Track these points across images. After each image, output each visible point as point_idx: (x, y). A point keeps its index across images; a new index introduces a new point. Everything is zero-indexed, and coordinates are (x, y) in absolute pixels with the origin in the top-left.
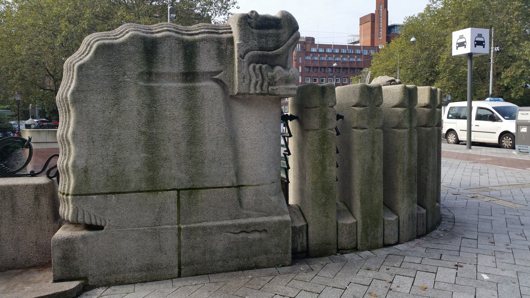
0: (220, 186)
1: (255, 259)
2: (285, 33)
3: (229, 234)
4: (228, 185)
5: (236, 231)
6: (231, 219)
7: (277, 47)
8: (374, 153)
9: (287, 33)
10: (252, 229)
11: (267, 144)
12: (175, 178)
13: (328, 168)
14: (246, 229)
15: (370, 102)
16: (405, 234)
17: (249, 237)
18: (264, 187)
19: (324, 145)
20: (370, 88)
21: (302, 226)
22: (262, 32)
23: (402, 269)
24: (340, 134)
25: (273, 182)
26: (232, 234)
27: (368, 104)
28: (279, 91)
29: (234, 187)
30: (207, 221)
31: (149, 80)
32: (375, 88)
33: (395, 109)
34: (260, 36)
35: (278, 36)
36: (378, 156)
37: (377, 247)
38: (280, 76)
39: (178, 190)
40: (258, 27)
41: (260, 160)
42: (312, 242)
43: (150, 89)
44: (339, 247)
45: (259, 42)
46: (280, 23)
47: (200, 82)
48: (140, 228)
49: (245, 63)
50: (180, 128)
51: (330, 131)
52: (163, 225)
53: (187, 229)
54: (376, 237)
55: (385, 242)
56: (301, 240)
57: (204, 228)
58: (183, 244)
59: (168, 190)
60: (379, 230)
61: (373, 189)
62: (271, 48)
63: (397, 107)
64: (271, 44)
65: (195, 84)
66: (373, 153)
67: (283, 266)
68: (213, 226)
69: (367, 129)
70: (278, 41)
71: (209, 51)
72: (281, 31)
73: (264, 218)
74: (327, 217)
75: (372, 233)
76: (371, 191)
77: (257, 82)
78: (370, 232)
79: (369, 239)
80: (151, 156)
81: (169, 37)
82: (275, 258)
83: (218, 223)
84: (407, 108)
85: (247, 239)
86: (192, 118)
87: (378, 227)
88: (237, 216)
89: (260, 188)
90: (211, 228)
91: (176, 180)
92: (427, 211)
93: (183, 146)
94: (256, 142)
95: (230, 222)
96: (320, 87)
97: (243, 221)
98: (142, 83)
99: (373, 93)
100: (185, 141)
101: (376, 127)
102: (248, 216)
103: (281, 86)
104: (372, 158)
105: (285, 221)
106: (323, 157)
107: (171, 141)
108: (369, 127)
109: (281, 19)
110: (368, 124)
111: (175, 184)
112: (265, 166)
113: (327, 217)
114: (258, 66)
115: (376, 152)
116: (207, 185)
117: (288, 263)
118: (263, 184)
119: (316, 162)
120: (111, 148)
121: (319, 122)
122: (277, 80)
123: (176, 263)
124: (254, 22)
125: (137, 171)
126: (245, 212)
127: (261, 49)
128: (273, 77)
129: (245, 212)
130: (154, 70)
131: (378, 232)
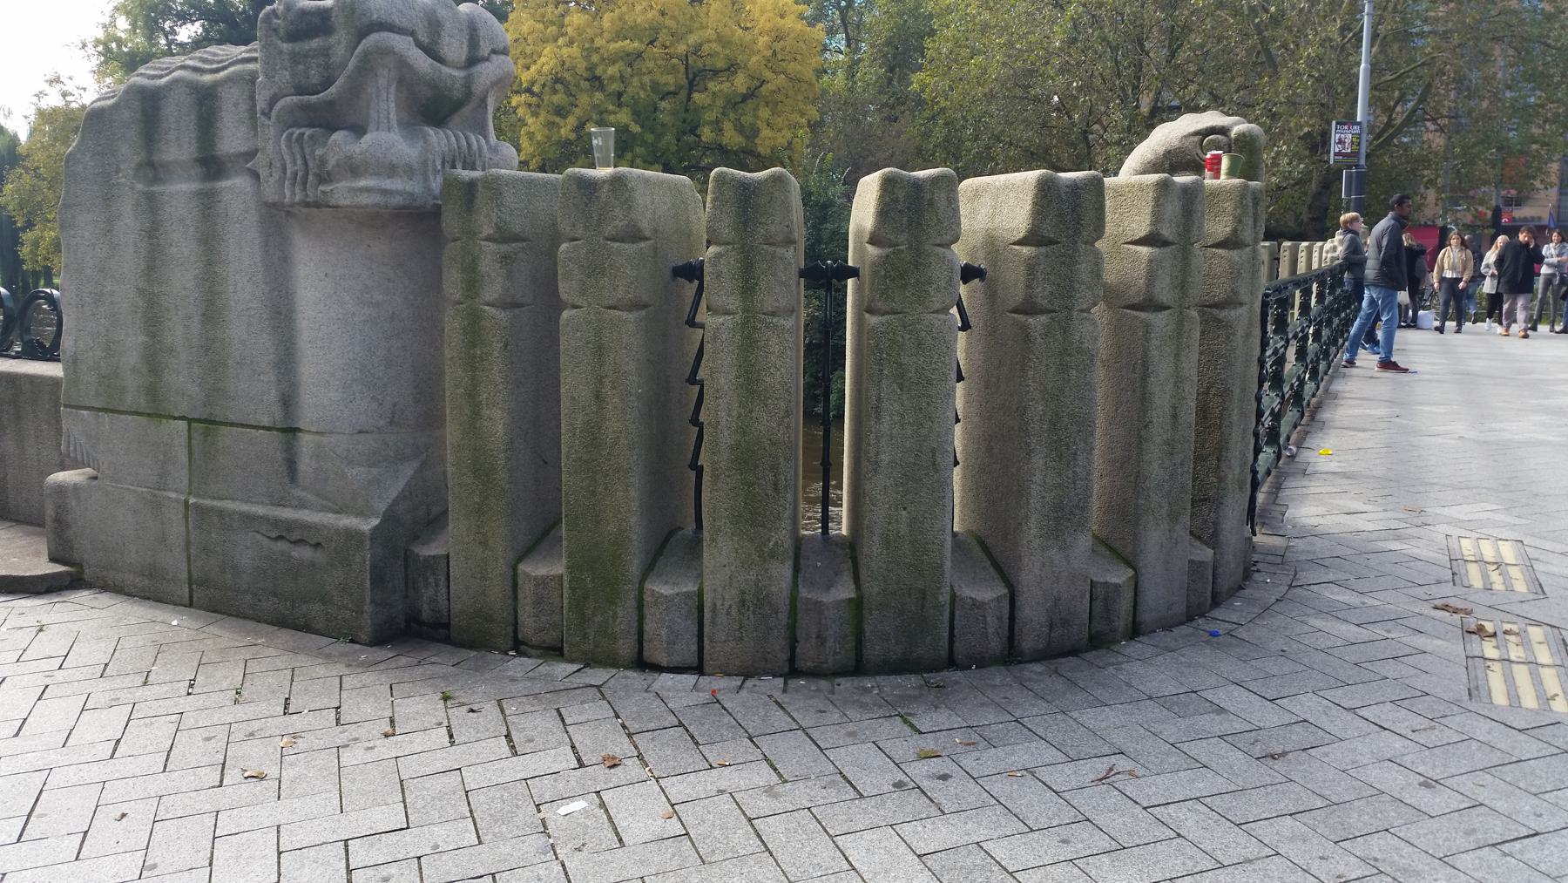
0: (252, 423)
1: (304, 608)
2: (339, 43)
3: (259, 537)
4: (267, 424)
5: (270, 534)
6: (272, 505)
7: (327, 82)
8: (601, 382)
9: (344, 44)
10: (296, 536)
11: (343, 333)
12: (183, 394)
13: (486, 412)
14: (287, 533)
15: (586, 228)
16: (720, 644)
17: (293, 554)
18: (333, 439)
19: (475, 346)
20: (590, 184)
21: (434, 557)
22: (297, 46)
23: (1341, 851)
24: (970, 327)
25: (360, 432)
26: (265, 539)
27: (579, 232)
28: (336, 196)
29: (278, 430)
30: (233, 499)
31: (156, 180)
32: (604, 182)
33: (1134, 247)
34: (295, 59)
35: (326, 52)
36: (614, 392)
37: (610, 662)
38: (336, 157)
39: (190, 421)
40: (293, 37)
41: (325, 373)
42: (456, 607)
43: (151, 198)
44: (786, 669)
45: (293, 75)
46: (328, 18)
47: (227, 178)
48: (139, 489)
49: (271, 129)
50: (191, 285)
51: (487, 308)
52: (169, 490)
53: (196, 506)
54: (610, 631)
55: (645, 653)
56: (431, 592)
57: (221, 513)
58: (192, 537)
59: (175, 418)
60: (620, 614)
61: (601, 489)
62: (316, 85)
63: (1141, 245)
64: (315, 77)
65: (202, 187)
66: (600, 380)
67: (352, 641)
68: (235, 512)
69: (580, 307)
70: (327, 67)
71: (236, 105)
72: (332, 40)
73: (331, 515)
74: (484, 544)
75: (599, 619)
76: (593, 493)
77: (296, 174)
78: (594, 615)
79: (591, 633)
80: (151, 343)
81: (176, 81)
82: (340, 617)
83: (244, 508)
84: (730, 247)
85: (290, 557)
86: (210, 263)
87: (615, 604)
88: (282, 499)
89: (325, 440)
90: (232, 514)
91: (186, 398)
92: (519, 560)
93: (195, 326)
94: (317, 326)
95: (260, 510)
96: (463, 183)
97: (287, 514)
98: (140, 187)
99: (597, 197)
100: (199, 312)
101: (607, 303)
102: (302, 505)
103: (344, 184)
104: (597, 397)
105: (357, 533)
106: (473, 379)
107: (179, 313)
108: (585, 303)
109: (331, 9)
110: (583, 292)
111: (184, 408)
112: (335, 388)
113: (484, 544)
114: (297, 131)
115: (607, 380)
116: (233, 418)
117: (364, 637)
118: (331, 433)
119: (458, 391)
120: (103, 321)
121: (462, 282)
122: (329, 167)
123: (185, 575)
124: (283, 25)
125: (134, 370)
126: (298, 493)
127: (300, 91)
128: (323, 162)
129: (298, 493)
130: (156, 158)
131: (615, 617)
